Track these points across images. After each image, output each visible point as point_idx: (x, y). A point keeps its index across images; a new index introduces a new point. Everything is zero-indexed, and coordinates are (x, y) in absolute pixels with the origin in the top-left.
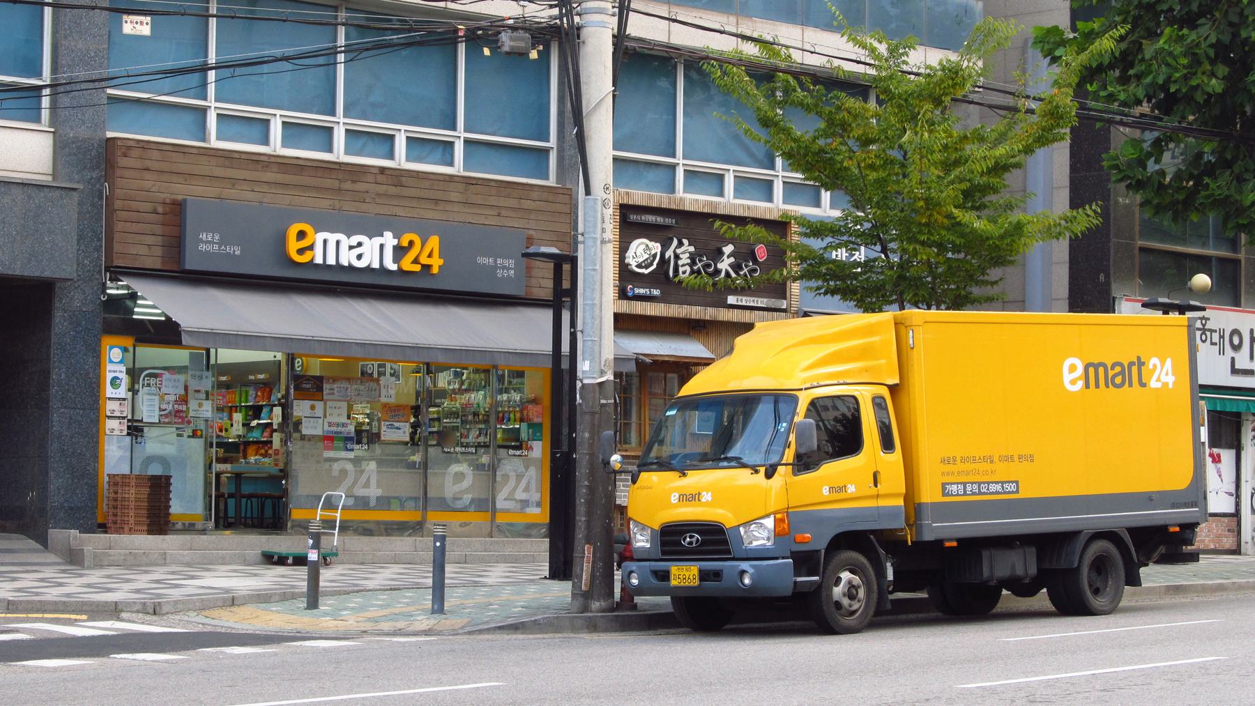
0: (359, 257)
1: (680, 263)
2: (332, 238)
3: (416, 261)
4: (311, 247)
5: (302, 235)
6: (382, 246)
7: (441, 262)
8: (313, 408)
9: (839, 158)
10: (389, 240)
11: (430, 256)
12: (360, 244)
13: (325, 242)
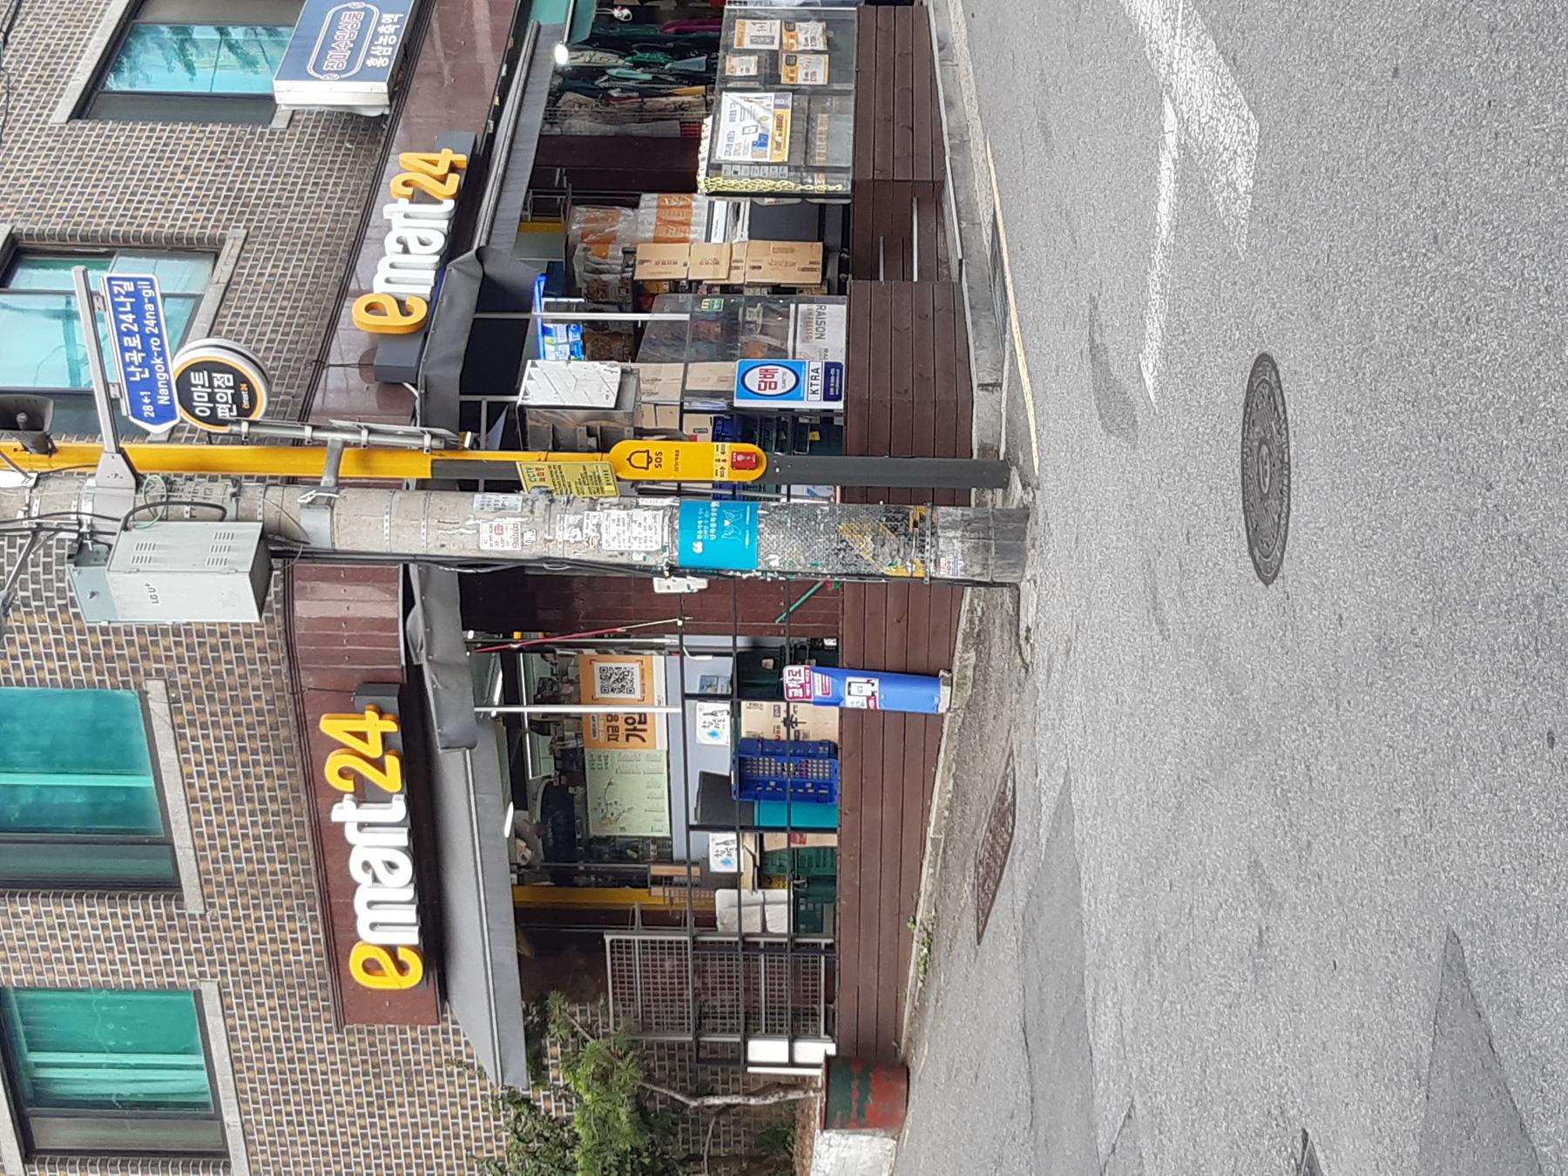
0: (391, 866)
1: (381, 29)
2: (364, 917)
3: (379, 764)
4: (391, 950)
5: (371, 967)
6: (361, 826)
7: (371, 715)
8: (530, 378)
9: (144, 230)
10: (345, 812)
11: (362, 736)
12: (366, 866)
13: (373, 926)
